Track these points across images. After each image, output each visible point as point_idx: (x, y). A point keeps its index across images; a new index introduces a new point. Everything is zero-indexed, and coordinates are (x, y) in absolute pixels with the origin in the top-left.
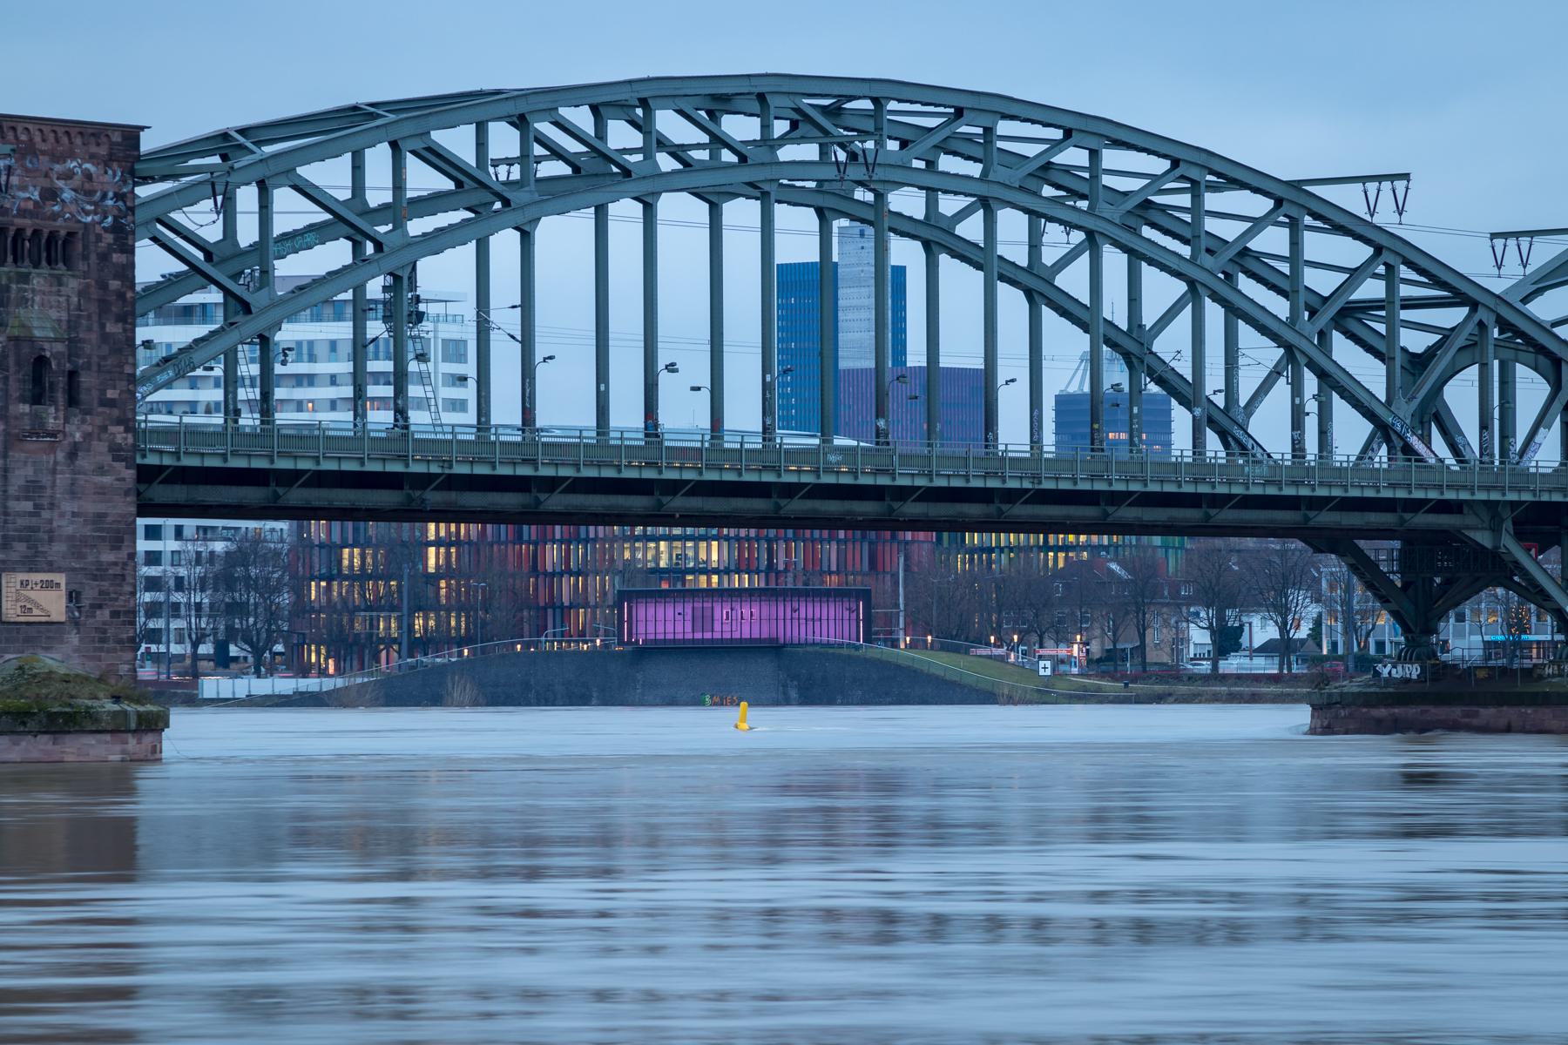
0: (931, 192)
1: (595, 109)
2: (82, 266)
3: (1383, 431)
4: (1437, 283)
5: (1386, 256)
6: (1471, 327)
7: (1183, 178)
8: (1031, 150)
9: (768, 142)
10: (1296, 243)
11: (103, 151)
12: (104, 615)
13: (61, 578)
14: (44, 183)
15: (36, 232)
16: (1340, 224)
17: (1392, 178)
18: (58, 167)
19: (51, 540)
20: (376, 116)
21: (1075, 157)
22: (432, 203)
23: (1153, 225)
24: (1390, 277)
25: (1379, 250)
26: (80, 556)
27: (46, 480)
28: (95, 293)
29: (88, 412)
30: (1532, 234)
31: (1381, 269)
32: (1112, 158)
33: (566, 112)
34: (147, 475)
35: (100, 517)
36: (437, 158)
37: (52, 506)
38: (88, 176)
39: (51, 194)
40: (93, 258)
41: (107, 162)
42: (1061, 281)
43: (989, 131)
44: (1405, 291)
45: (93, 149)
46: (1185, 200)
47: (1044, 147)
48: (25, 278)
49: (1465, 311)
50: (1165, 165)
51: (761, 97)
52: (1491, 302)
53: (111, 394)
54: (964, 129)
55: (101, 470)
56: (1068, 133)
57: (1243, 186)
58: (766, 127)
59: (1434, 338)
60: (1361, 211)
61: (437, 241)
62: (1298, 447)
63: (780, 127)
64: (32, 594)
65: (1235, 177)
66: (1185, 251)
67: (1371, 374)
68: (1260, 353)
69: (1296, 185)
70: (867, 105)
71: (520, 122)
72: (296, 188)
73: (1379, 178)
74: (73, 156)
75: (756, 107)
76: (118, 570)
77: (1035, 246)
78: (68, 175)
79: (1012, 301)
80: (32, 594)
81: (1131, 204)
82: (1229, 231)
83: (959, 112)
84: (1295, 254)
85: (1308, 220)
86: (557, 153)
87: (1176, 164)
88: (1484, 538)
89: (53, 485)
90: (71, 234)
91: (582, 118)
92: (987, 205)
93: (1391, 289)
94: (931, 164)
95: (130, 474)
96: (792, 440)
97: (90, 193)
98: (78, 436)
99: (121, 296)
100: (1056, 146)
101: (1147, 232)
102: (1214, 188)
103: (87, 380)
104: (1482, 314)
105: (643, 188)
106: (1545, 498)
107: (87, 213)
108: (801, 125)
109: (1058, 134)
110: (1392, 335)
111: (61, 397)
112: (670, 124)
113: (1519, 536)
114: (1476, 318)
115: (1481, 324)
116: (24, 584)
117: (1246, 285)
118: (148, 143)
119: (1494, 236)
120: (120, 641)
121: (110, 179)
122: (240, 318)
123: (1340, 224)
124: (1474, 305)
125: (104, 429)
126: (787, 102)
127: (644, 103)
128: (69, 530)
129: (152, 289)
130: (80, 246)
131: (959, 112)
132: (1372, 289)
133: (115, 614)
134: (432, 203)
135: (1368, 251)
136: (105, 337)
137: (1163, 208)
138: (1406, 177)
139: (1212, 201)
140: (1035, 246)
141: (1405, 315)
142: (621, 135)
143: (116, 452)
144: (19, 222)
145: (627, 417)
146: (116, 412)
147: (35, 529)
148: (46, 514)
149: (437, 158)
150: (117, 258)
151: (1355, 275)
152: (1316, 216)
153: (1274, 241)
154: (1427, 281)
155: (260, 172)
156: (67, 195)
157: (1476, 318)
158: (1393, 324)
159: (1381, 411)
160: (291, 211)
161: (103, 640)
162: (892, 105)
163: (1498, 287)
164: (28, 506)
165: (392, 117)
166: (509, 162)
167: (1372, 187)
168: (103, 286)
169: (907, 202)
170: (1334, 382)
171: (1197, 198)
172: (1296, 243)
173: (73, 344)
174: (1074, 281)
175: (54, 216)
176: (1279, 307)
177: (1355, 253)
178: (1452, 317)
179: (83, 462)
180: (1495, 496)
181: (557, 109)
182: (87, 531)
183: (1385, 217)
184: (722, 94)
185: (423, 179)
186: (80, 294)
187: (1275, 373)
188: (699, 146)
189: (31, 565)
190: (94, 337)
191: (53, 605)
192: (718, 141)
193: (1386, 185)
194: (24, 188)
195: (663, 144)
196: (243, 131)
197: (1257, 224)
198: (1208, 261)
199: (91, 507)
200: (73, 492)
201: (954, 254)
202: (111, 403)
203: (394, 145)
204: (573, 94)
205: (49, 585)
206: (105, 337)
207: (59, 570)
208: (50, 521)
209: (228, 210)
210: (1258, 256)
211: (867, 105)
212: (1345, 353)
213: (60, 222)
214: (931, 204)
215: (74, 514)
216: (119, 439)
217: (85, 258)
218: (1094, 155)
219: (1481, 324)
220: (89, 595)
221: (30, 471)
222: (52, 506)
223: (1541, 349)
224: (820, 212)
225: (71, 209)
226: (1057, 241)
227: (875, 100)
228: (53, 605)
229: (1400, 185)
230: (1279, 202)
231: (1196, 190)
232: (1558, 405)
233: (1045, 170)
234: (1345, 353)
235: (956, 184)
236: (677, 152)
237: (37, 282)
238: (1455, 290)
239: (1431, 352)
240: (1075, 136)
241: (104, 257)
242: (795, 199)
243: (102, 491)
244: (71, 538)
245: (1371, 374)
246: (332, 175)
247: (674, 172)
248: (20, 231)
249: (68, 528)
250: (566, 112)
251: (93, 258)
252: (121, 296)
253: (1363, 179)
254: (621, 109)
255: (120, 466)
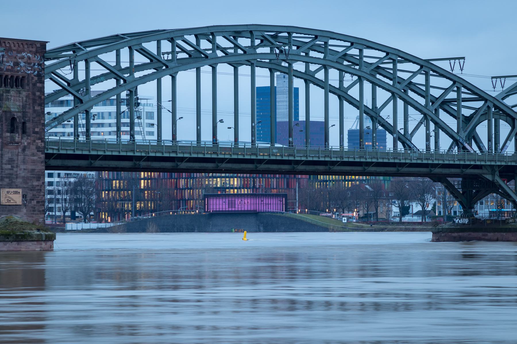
0: (307, 63)
1: (196, 36)
2: (27, 88)
3: (456, 142)
4: (474, 93)
5: (457, 84)
6: (485, 108)
7: (390, 59)
8: (340, 49)
9: (253, 47)
10: (427, 80)
11: (34, 50)
12: (34, 202)
13: (20, 190)
14: (15, 60)
15: (12, 77)
16: (442, 74)
17: (459, 58)
18: (19, 55)
19: (17, 178)
20: (124, 38)
21: (354, 52)
22: (142, 67)
23: (380, 74)
24: (458, 91)
25: (455, 82)
26: (26, 183)
27: (15, 158)
28: (31, 96)
29: (29, 136)
30: (505, 77)
31: (455, 89)
32: (367, 52)
33: (186, 37)
34: (48, 156)
35: (33, 170)
36: (144, 52)
37: (17, 166)
38: (29, 58)
39: (17, 64)
40: (31, 85)
41: (35, 53)
42: (350, 92)
43: (326, 43)
44: (463, 96)
45: (31, 49)
46: (391, 66)
47: (344, 48)
48: (8, 92)
49: (483, 102)
50: (384, 54)
51: (251, 32)
52: (492, 100)
53: (37, 130)
54: (318, 42)
55: (33, 155)
56: (352, 44)
57: (410, 61)
58: (253, 42)
59: (473, 111)
60: (449, 69)
61: (144, 79)
62: (428, 147)
63: (257, 42)
64: (11, 196)
65: (407, 58)
66: (391, 83)
67: (452, 123)
68: (415, 116)
69: (427, 61)
70: (286, 34)
71: (172, 40)
72: (98, 62)
73: (455, 59)
74: (24, 51)
75: (249, 35)
76: (39, 188)
77: (341, 81)
78: (23, 58)
79: (334, 99)
80: (11, 196)
81: (373, 67)
82: (405, 76)
83: (316, 37)
84: (427, 84)
85: (431, 72)
86: (184, 50)
87: (388, 54)
88: (489, 177)
89: (18, 160)
90: (23, 77)
91: (192, 39)
92: (325, 67)
93: (459, 95)
94: (307, 54)
95: (43, 156)
96: (261, 145)
97: (30, 64)
98: (26, 144)
99: (40, 97)
100: (348, 48)
101: (378, 76)
102: (400, 62)
103: (29, 125)
104: (489, 103)
105: (212, 62)
106: (509, 164)
107: (29, 70)
108: (264, 41)
109: (349, 44)
110: (459, 110)
111: (20, 131)
112: (221, 41)
113: (501, 176)
114: (487, 105)
115: (488, 107)
116: (8, 192)
117: (411, 94)
118: (49, 47)
119: (493, 78)
120: (40, 211)
121: (36, 59)
122: (79, 105)
123: (442, 74)
124: (486, 101)
125: (34, 141)
126: (260, 34)
127: (212, 34)
128: (23, 174)
129: (50, 95)
130: (26, 81)
131: (316, 37)
132: (452, 95)
133: (38, 202)
134: (142, 67)
135: (451, 83)
136: (35, 111)
137: (384, 69)
138: (464, 58)
139: (400, 66)
140: (341, 81)
141: (463, 104)
142: (205, 45)
143: (38, 149)
144: (6, 73)
145: (207, 137)
146: (38, 136)
147: (12, 174)
148: (15, 169)
149: (144, 52)
150: (39, 85)
151: (447, 91)
152: (434, 71)
153: (420, 79)
154: (470, 92)
155: (86, 57)
156: (22, 64)
157: (487, 105)
158: (459, 107)
159: (455, 135)
160: (96, 70)
161: (34, 211)
162: (294, 35)
163: (494, 95)
164: (9, 166)
165: (129, 38)
166: (168, 53)
167: (452, 61)
168: (34, 94)
169: (299, 66)
170: (440, 126)
171: (395, 65)
172: (427, 80)
173: (24, 113)
174: (354, 92)
175: (18, 71)
176: (422, 101)
177: (447, 83)
178: (479, 104)
179: (27, 152)
180: (493, 163)
181: (184, 36)
182: (29, 175)
183: (457, 71)
184: (238, 31)
185: (139, 59)
186: (27, 97)
187: (421, 123)
188: (230, 48)
189: (10, 186)
190: (31, 111)
191: (18, 199)
192: (237, 47)
193: (457, 61)
194: (8, 62)
195: (218, 47)
196: (80, 43)
197: (415, 74)
198: (398, 86)
199: (30, 167)
200: (24, 162)
201: (315, 84)
202: (37, 133)
203: (130, 48)
204: (189, 31)
205: (16, 193)
206: (35, 111)
207: (20, 188)
208: (17, 172)
209: (75, 69)
210: (415, 84)
211: (286, 34)
212: (444, 116)
213: (20, 73)
214: (307, 67)
215: (24, 169)
216: (39, 145)
217: (28, 85)
218: (361, 51)
219: (488, 107)
220: (29, 196)
221: (10, 155)
222: (17, 166)
223: (508, 115)
224: (270, 70)
225: (23, 69)
226: (348, 79)
227: (289, 33)
228: (18, 199)
229: (462, 61)
230: (422, 67)
231: (394, 62)
232: (514, 133)
233: (345, 56)
234: (444, 116)
235: (315, 61)
236: (223, 50)
237: (12, 93)
238: (480, 96)
239: (472, 116)
240: (355, 45)
241: (34, 85)
242: (262, 65)
243: (33, 162)
244: (23, 177)
245: (452, 123)
246: (109, 58)
247: (222, 57)
248: (6, 76)
249: (22, 174)
250: (186, 37)
251: (31, 85)
252: (40, 97)
253: (449, 59)
254: (205, 36)
255: (39, 153)
